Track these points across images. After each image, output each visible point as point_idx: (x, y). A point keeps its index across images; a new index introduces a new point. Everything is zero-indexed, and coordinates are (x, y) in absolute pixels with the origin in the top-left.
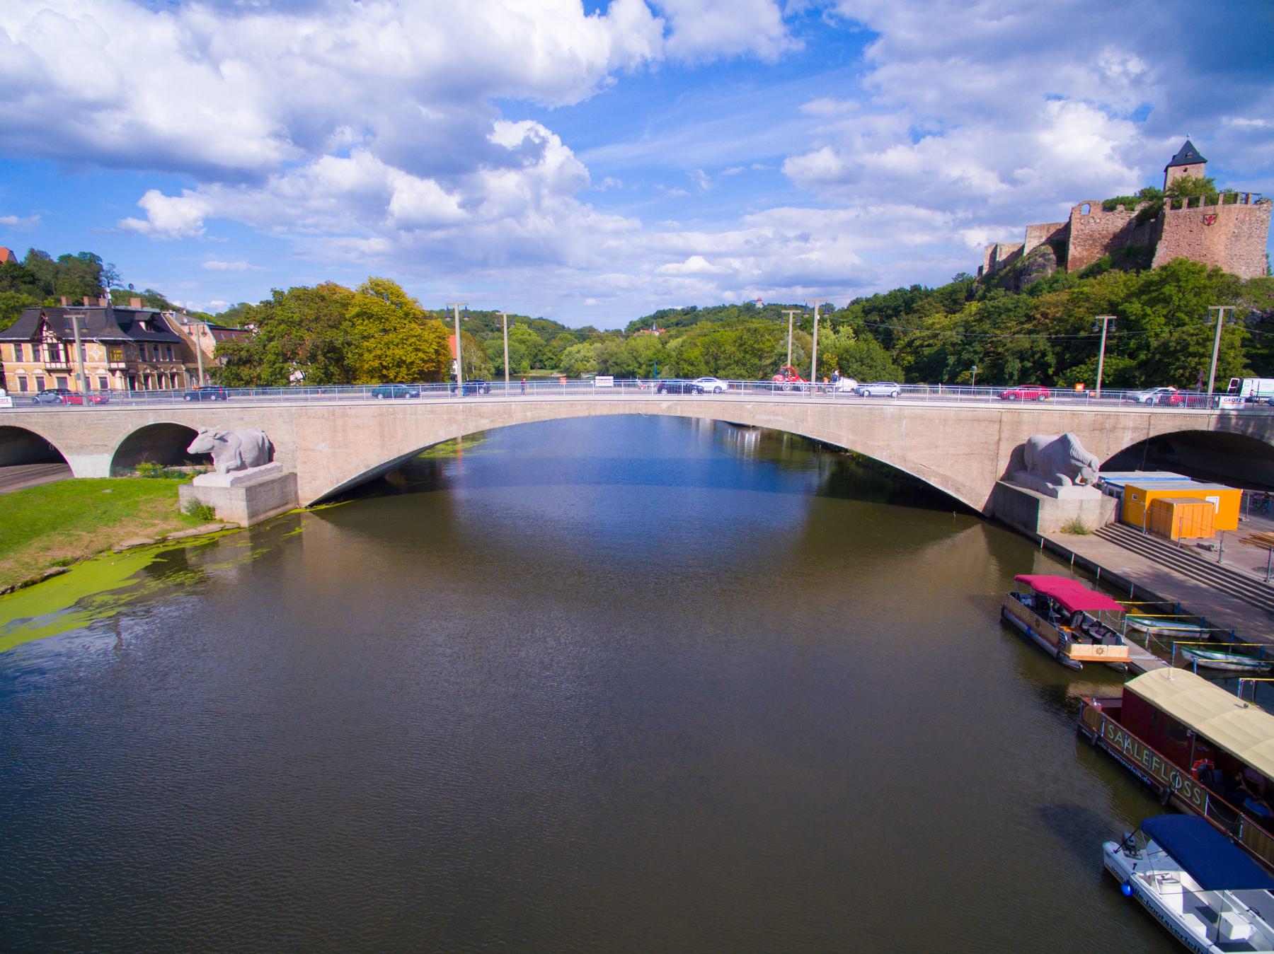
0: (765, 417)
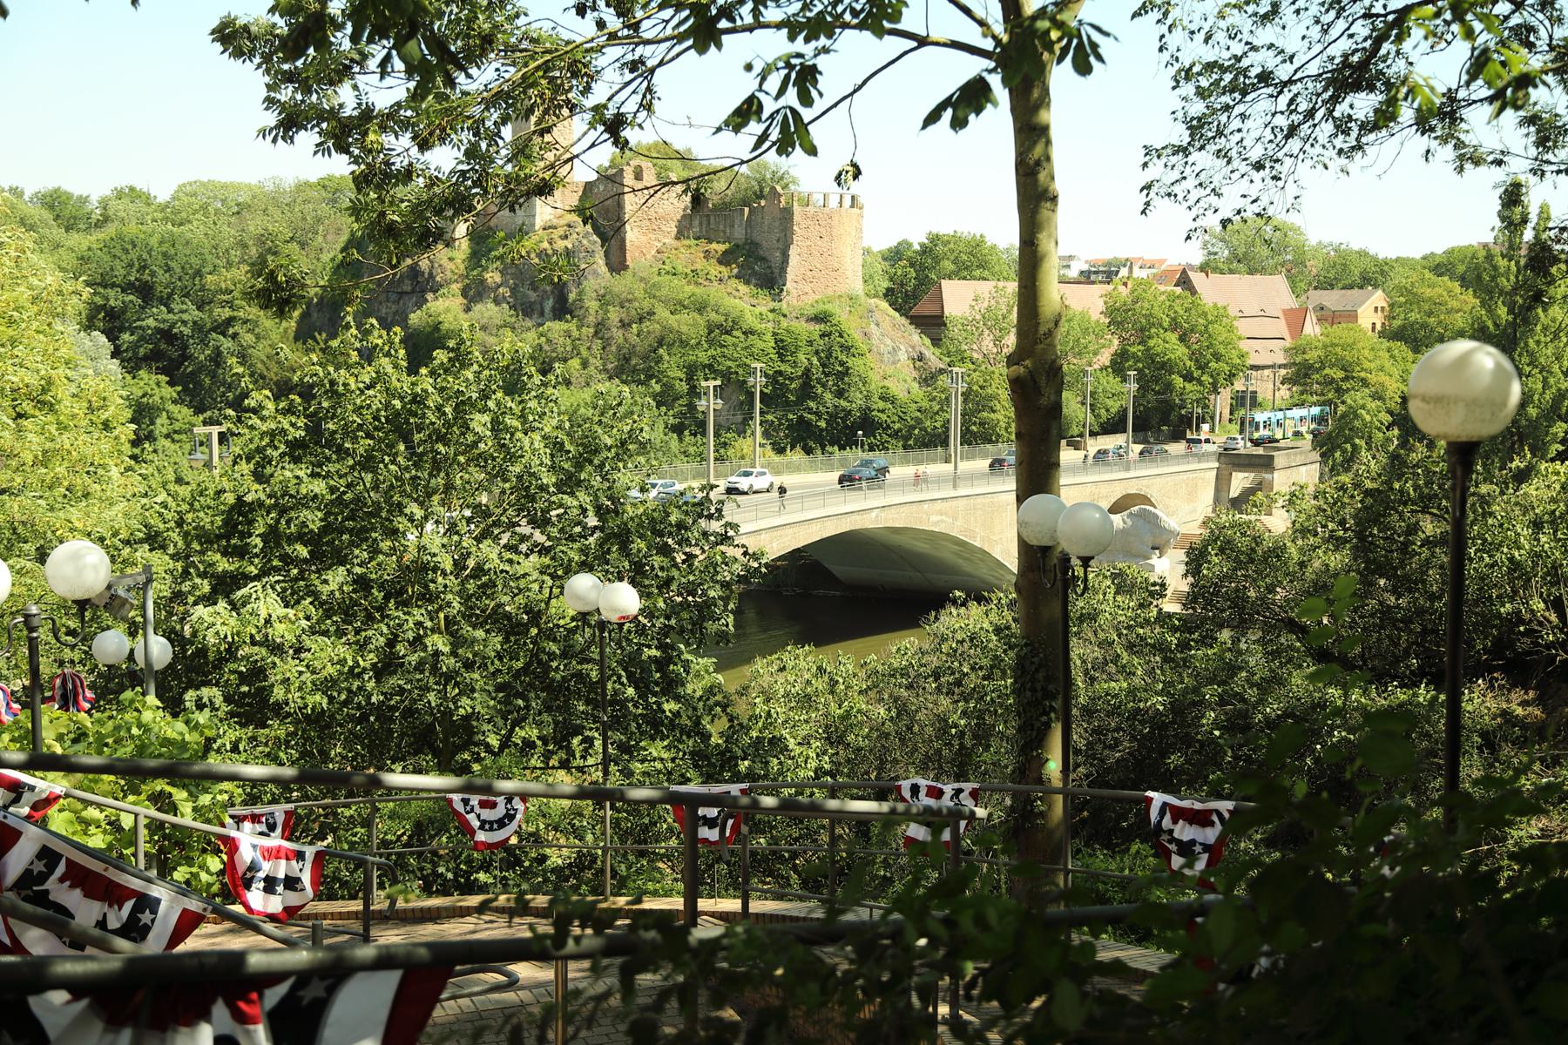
0: (934, 518)
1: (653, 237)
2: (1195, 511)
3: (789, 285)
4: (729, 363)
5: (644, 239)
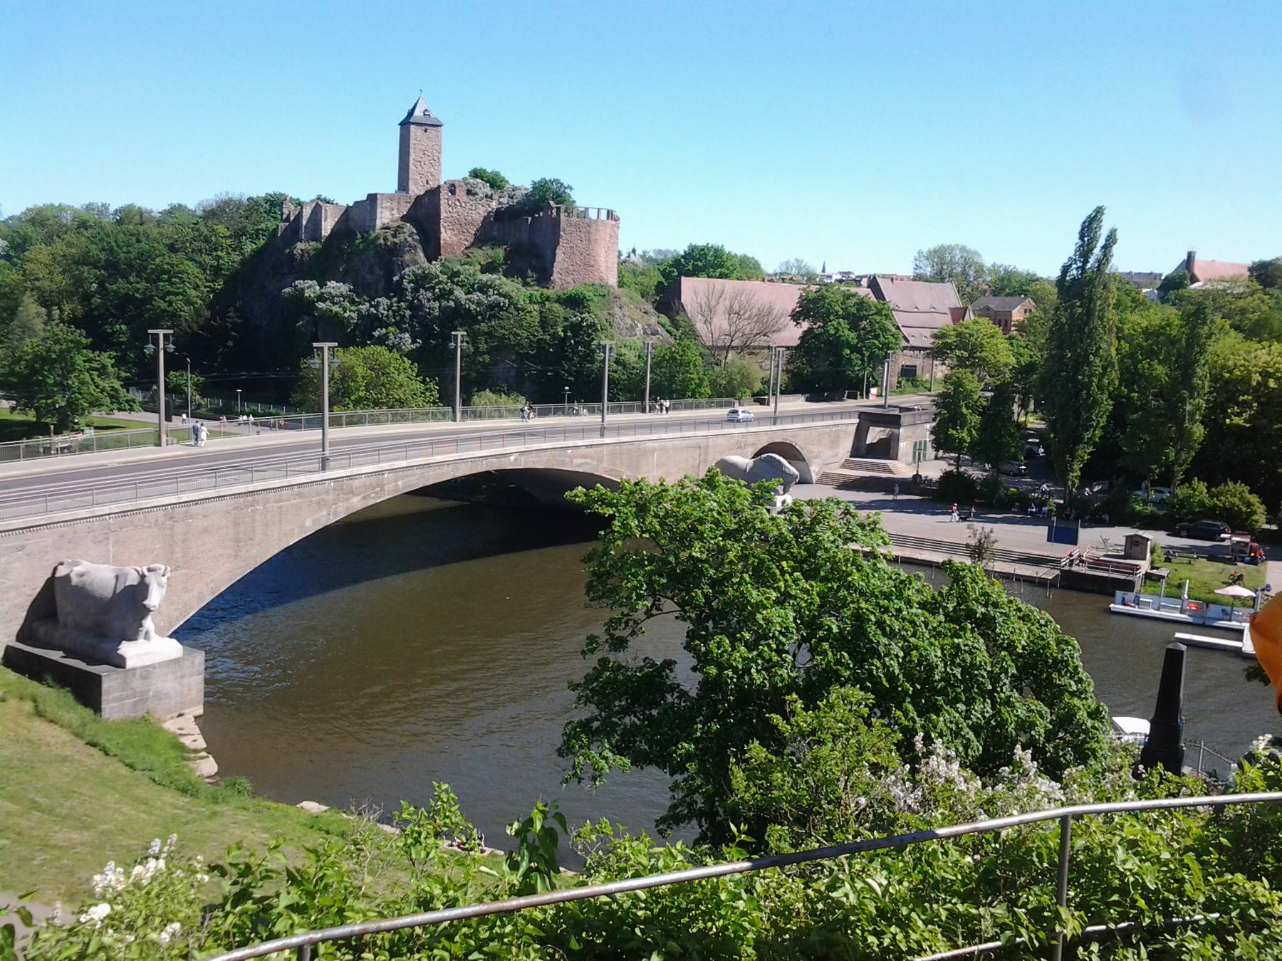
0: (577, 461)
1: (463, 238)
2: (837, 455)
3: (555, 277)
4: (503, 331)
5: (455, 239)
